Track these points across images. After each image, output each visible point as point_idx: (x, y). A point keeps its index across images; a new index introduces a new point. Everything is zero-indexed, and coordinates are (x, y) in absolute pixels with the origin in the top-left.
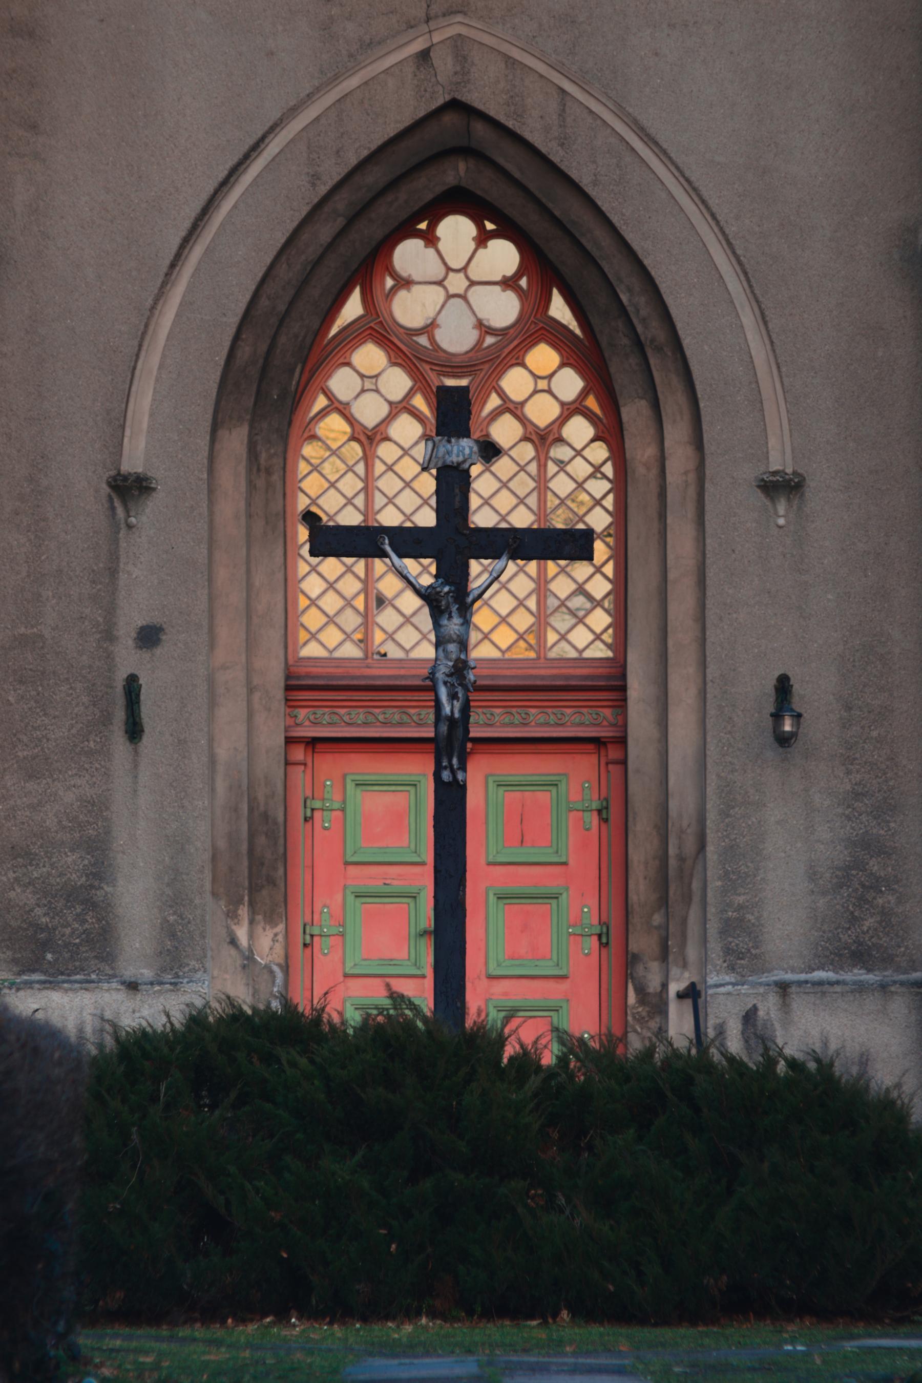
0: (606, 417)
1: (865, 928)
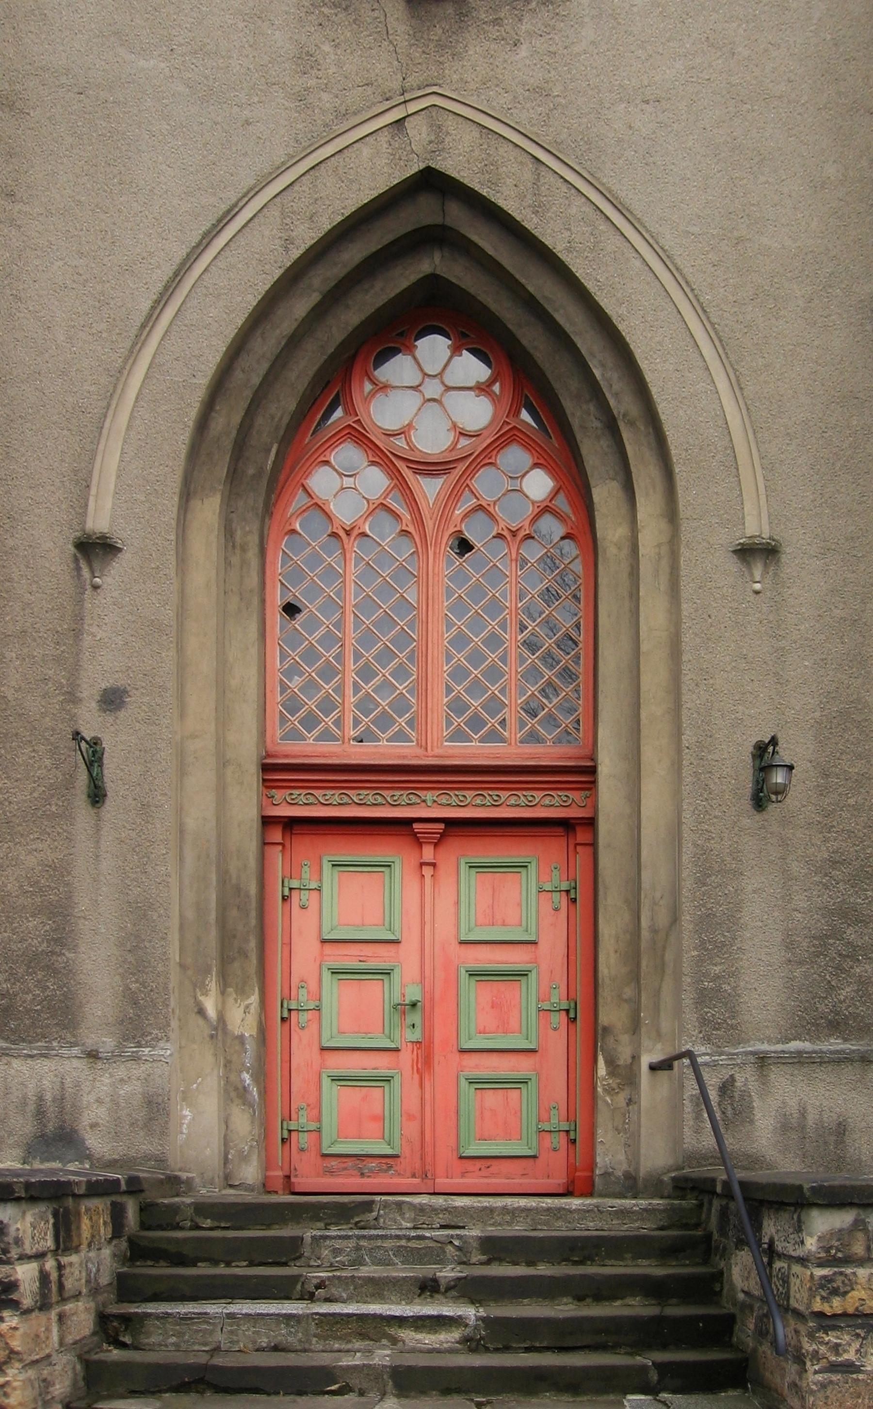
0: (574, 514)
1: (842, 998)
